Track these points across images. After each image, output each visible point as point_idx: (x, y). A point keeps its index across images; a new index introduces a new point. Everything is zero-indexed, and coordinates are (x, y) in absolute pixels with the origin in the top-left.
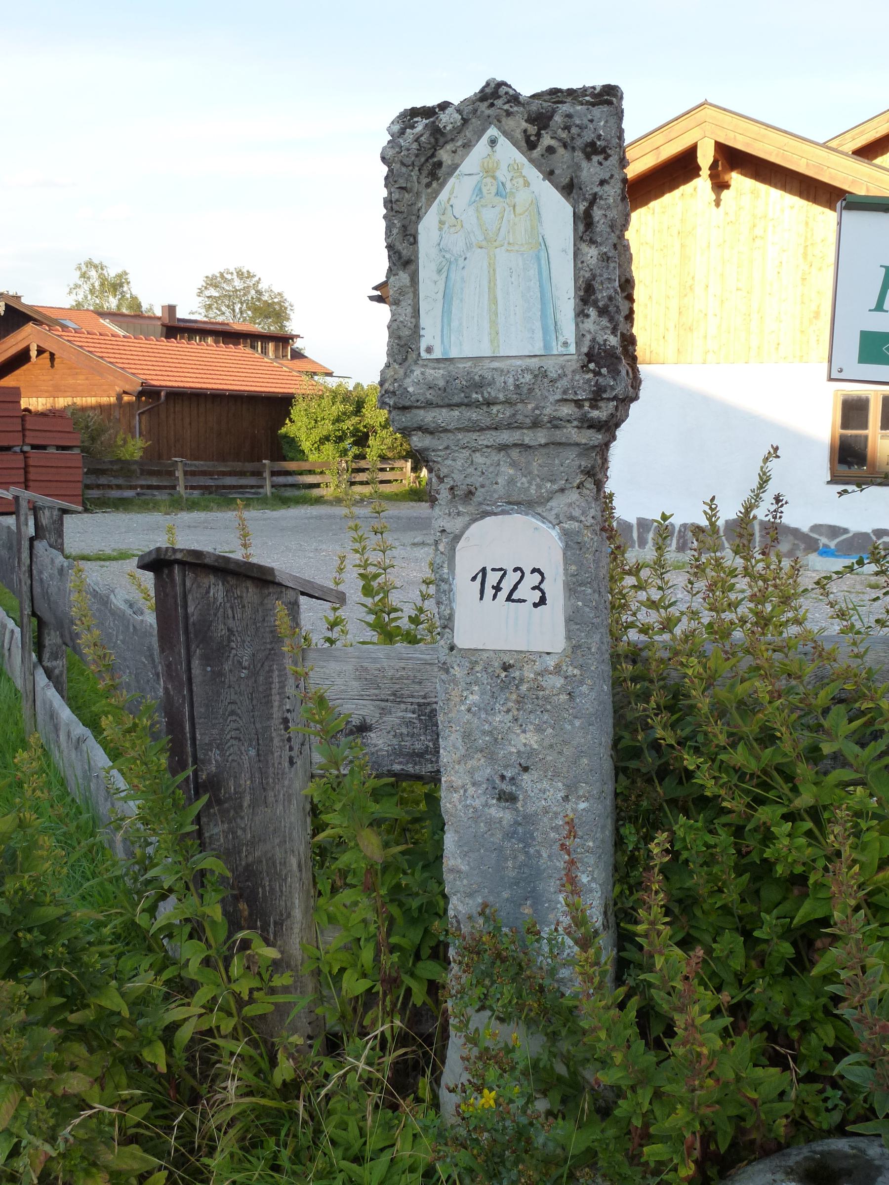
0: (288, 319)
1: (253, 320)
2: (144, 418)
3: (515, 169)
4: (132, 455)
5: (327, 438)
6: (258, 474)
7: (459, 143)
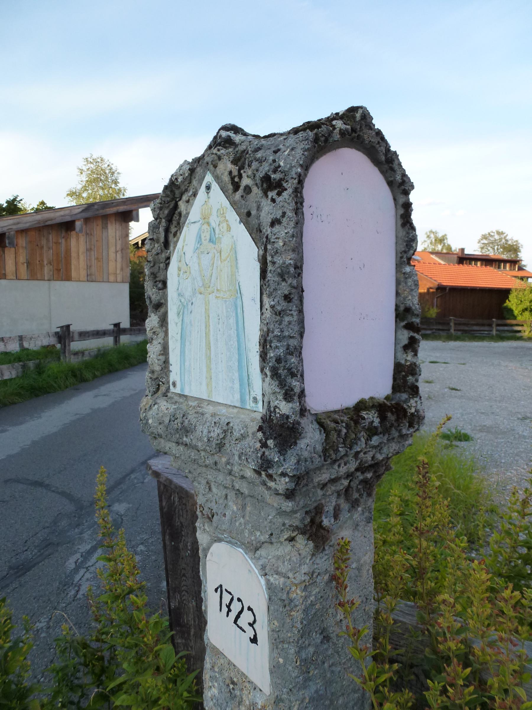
0: (520, 252)
1: (503, 253)
2: (439, 299)
3: (221, 214)
4: (431, 315)
5: (526, 309)
6: (490, 325)
7: (191, 193)
